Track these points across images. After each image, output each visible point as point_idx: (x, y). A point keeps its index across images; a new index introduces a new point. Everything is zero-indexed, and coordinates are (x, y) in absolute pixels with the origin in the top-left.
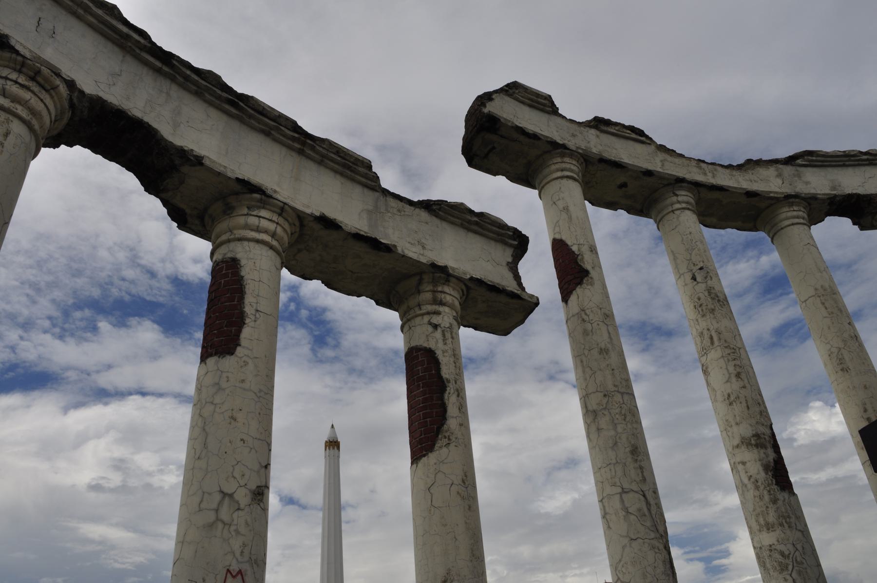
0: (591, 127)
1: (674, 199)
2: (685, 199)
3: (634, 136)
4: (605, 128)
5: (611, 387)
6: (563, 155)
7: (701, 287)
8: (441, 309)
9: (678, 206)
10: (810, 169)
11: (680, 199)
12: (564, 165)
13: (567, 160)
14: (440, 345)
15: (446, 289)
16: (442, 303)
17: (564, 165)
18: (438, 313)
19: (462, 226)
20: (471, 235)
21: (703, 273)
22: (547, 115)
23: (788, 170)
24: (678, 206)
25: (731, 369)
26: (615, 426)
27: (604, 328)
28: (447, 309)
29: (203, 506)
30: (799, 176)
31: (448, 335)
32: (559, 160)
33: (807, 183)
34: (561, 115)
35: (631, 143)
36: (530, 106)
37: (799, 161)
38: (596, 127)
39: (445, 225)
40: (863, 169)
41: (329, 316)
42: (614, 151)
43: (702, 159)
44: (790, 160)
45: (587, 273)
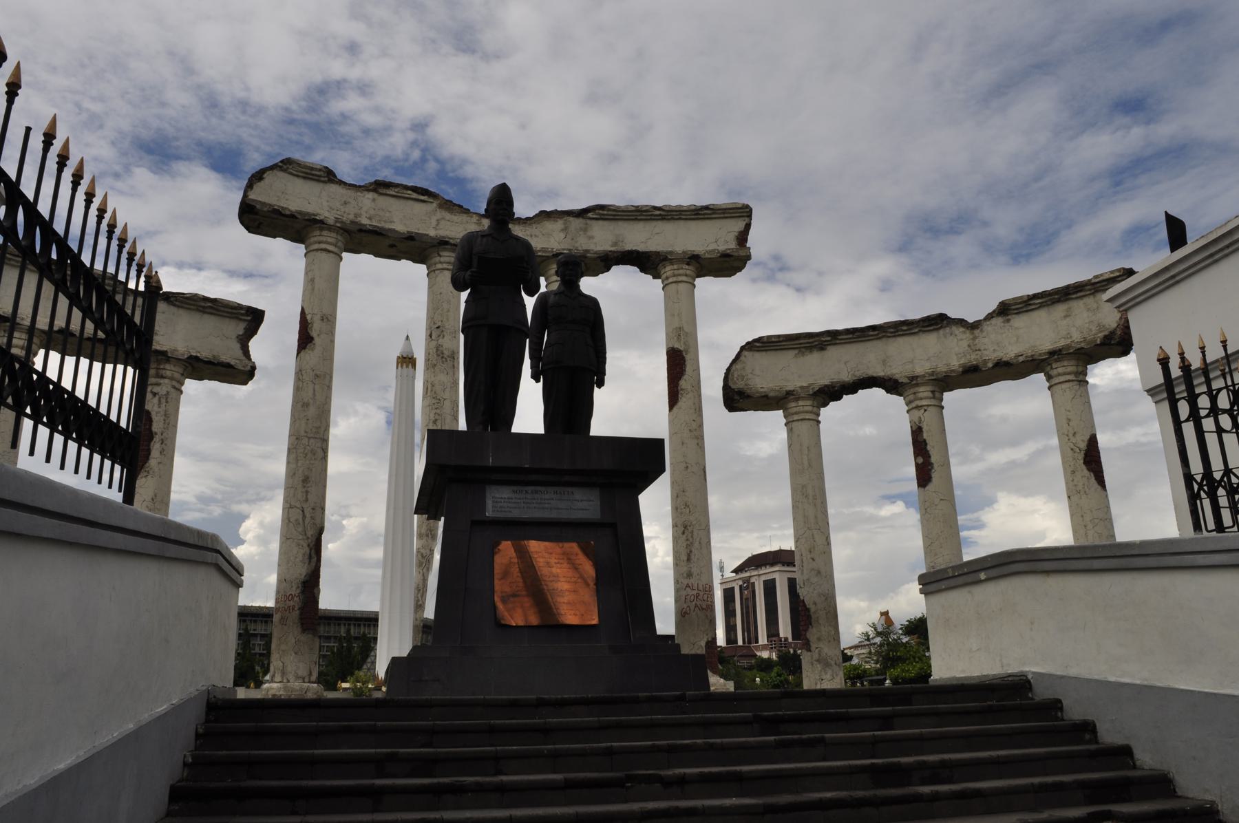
0: (369, 191)
1: (437, 259)
2: (447, 259)
3: (415, 196)
4: (384, 191)
5: (303, 433)
6: (321, 229)
7: (434, 343)
8: (162, 381)
9: (439, 266)
10: (601, 222)
11: (442, 259)
12: (321, 239)
13: (325, 233)
14: (156, 408)
15: (167, 366)
16: (162, 377)
17: (321, 239)
18: (158, 384)
19: (198, 310)
20: (206, 316)
21: (438, 332)
22: (321, 185)
23: (576, 223)
24: (439, 266)
25: (432, 415)
26: (297, 460)
27: (311, 386)
28: (166, 381)
29: (739, 225)
30: (585, 230)
31: (163, 401)
32: (318, 233)
33: (591, 238)
34: (341, 183)
35: (411, 202)
36: (304, 178)
37: (590, 215)
38: (375, 190)
39: (181, 311)
40: (654, 223)
41: (469, 171)
42: (388, 214)
43: (205, 354)
44: (582, 213)
45: (312, 339)
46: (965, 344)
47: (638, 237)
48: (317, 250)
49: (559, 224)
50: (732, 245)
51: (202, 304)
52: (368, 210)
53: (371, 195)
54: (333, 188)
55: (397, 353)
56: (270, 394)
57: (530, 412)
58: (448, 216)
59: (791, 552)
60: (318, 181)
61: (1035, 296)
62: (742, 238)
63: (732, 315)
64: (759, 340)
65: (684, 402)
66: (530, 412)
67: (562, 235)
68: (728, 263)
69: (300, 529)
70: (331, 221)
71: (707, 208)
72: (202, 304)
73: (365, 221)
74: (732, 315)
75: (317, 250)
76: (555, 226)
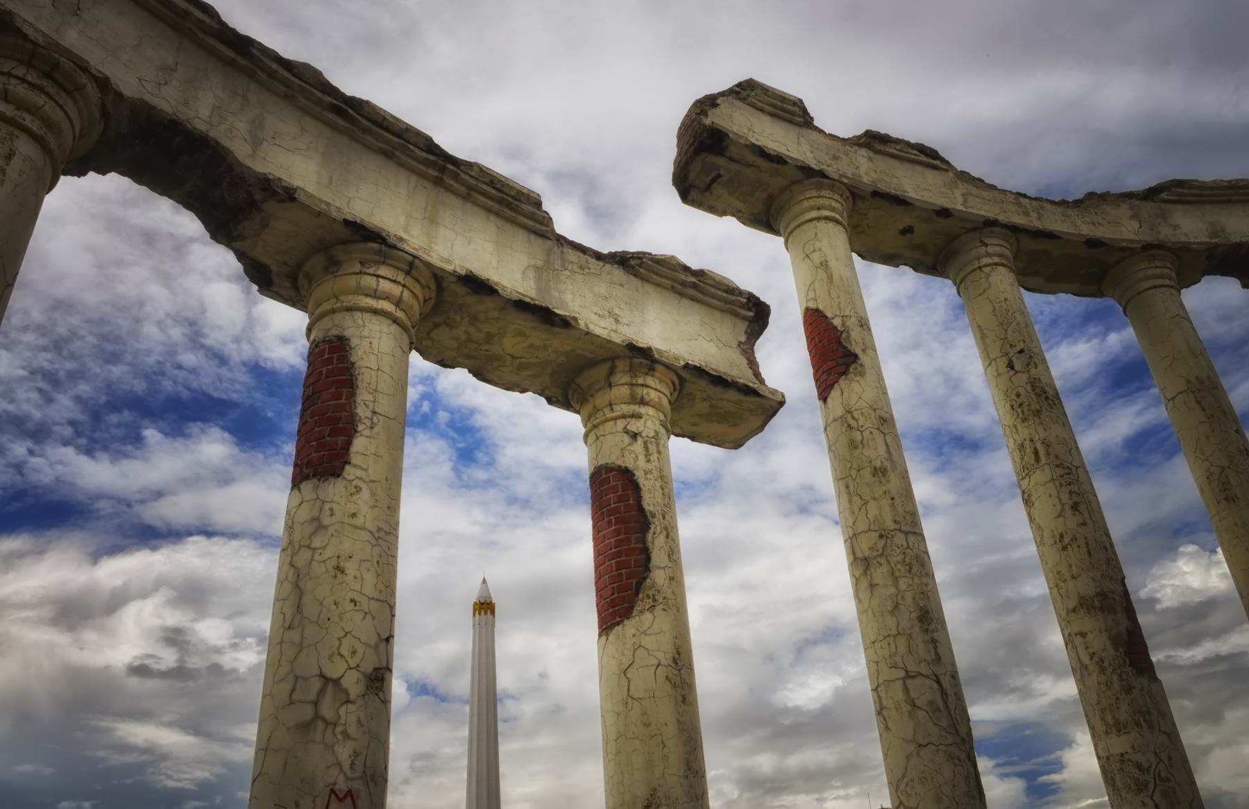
0: (860, 145)
1: (982, 250)
3: (923, 158)
5: (890, 524)
6: (820, 187)
8: (643, 410)
10: (1179, 207)
11: (990, 250)
12: (821, 201)
13: (825, 193)
15: (650, 381)
16: (643, 402)
23: (1147, 208)
25: (1065, 497)
27: (879, 438)
33: (1176, 227)
35: (919, 168)
36: (772, 115)
37: (1164, 196)
42: (894, 180)
48: (818, 219)
51: (682, 277)
55: (474, 599)
56: (796, 452)
60: (790, 121)
67: (1135, 225)
69: (944, 723)
72: (682, 277)
75: (818, 219)
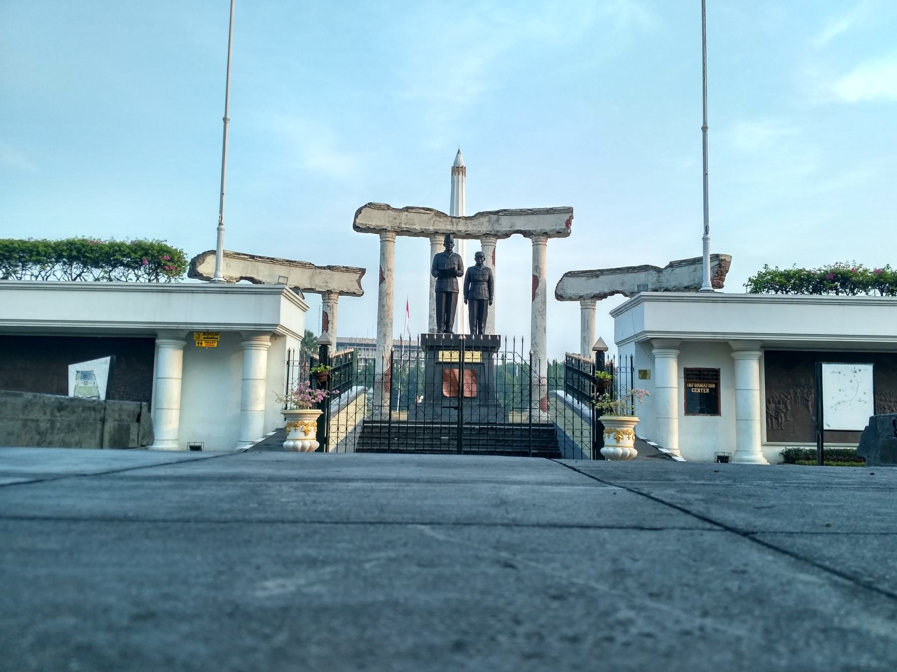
23: (494, 217)
29: (567, 217)
46: (655, 278)
47: (521, 223)
49: (487, 219)
50: (564, 226)
52: (404, 220)
53: (406, 213)
54: (390, 211)
57: (462, 326)
58: (438, 219)
59: (147, 438)
61: (683, 261)
62: (568, 223)
63: (561, 258)
64: (570, 272)
65: (538, 299)
66: (462, 326)
68: (563, 233)
70: (499, 527)
71: (552, 209)
73: (403, 226)
74: (561, 258)
76: (484, 220)
